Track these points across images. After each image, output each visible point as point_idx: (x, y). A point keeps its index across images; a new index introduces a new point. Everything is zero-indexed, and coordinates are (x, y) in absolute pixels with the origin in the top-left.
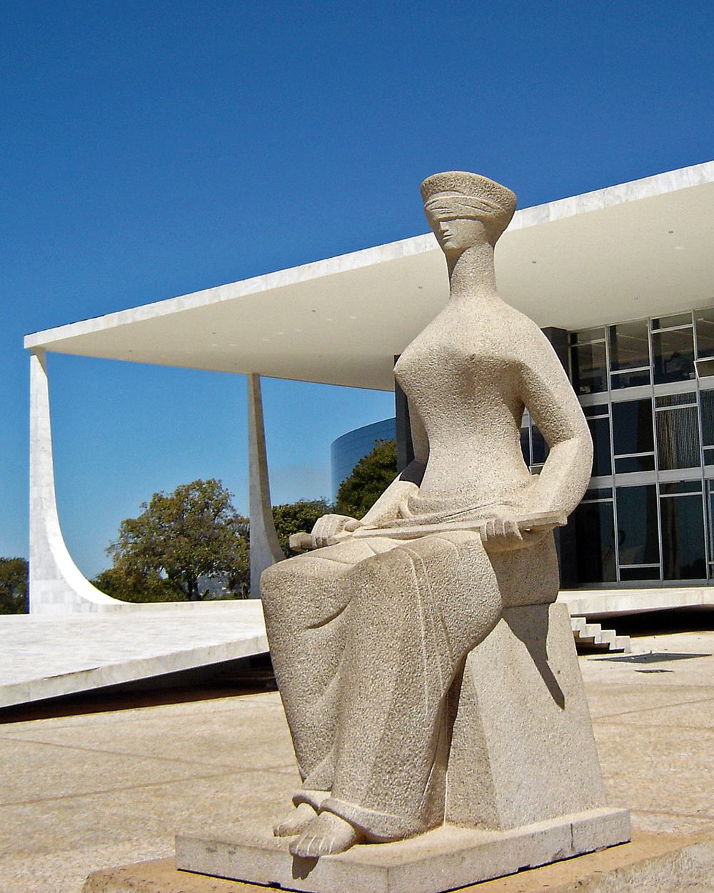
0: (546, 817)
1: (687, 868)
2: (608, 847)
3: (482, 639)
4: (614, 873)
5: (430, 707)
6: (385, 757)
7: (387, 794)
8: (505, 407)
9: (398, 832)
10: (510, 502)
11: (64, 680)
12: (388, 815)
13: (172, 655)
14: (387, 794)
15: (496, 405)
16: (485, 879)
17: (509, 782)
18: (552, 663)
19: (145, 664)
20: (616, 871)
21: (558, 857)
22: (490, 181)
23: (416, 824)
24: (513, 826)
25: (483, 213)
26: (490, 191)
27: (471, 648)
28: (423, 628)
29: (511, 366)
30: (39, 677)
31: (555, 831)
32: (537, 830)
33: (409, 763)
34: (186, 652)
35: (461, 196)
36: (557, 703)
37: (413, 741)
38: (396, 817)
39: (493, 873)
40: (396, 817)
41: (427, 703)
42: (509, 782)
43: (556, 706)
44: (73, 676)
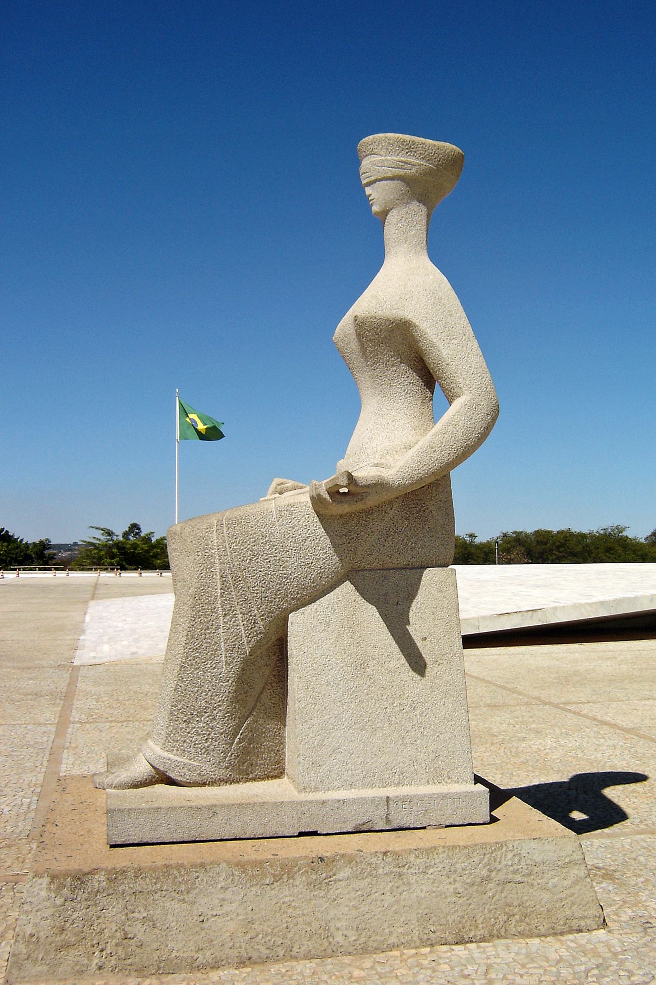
0: (364, 786)
1: (510, 863)
2: (447, 826)
3: (313, 600)
4: (381, 856)
5: (227, 664)
6: (179, 707)
7: (184, 742)
8: (403, 367)
9: (198, 779)
10: (382, 464)
11: (510, 616)
12: (188, 761)
13: (614, 600)
14: (184, 742)
15: (393, 366)
16: (246, 836)
17: (321, 745)
18: (416, 629)
19: (588, 607)
20: (385, 853)
21: (365, 828)
22: (407, 137)
23: (222, 773)
24: (316, 789)
25: (402, 172)
26: (410, 148)
27: (296, 609)
28: (219, 586)
29: (397, 325)
30: (488, 613)
31: (362, 801)
32: (329, 798)
33: (206, 715)
34: (629, 598)
35: (379, 158)
36: (415, 670)
37: (210, 694)
38: (196, 764)
39: (259, 833)
40: (196, 764)
41: (223, 659)
42: (321, 745)
43: (412, 673)
44: (506, 617)
